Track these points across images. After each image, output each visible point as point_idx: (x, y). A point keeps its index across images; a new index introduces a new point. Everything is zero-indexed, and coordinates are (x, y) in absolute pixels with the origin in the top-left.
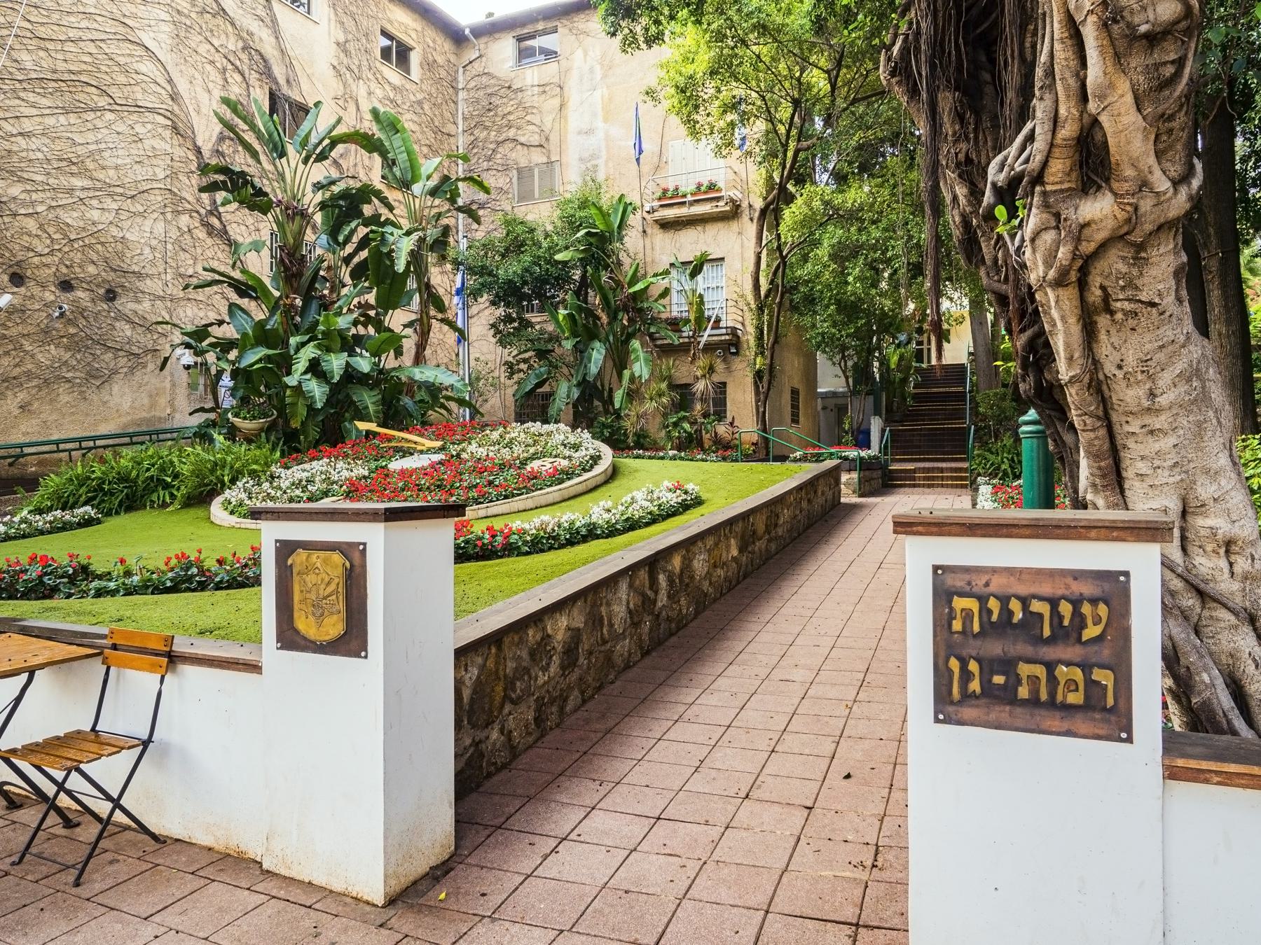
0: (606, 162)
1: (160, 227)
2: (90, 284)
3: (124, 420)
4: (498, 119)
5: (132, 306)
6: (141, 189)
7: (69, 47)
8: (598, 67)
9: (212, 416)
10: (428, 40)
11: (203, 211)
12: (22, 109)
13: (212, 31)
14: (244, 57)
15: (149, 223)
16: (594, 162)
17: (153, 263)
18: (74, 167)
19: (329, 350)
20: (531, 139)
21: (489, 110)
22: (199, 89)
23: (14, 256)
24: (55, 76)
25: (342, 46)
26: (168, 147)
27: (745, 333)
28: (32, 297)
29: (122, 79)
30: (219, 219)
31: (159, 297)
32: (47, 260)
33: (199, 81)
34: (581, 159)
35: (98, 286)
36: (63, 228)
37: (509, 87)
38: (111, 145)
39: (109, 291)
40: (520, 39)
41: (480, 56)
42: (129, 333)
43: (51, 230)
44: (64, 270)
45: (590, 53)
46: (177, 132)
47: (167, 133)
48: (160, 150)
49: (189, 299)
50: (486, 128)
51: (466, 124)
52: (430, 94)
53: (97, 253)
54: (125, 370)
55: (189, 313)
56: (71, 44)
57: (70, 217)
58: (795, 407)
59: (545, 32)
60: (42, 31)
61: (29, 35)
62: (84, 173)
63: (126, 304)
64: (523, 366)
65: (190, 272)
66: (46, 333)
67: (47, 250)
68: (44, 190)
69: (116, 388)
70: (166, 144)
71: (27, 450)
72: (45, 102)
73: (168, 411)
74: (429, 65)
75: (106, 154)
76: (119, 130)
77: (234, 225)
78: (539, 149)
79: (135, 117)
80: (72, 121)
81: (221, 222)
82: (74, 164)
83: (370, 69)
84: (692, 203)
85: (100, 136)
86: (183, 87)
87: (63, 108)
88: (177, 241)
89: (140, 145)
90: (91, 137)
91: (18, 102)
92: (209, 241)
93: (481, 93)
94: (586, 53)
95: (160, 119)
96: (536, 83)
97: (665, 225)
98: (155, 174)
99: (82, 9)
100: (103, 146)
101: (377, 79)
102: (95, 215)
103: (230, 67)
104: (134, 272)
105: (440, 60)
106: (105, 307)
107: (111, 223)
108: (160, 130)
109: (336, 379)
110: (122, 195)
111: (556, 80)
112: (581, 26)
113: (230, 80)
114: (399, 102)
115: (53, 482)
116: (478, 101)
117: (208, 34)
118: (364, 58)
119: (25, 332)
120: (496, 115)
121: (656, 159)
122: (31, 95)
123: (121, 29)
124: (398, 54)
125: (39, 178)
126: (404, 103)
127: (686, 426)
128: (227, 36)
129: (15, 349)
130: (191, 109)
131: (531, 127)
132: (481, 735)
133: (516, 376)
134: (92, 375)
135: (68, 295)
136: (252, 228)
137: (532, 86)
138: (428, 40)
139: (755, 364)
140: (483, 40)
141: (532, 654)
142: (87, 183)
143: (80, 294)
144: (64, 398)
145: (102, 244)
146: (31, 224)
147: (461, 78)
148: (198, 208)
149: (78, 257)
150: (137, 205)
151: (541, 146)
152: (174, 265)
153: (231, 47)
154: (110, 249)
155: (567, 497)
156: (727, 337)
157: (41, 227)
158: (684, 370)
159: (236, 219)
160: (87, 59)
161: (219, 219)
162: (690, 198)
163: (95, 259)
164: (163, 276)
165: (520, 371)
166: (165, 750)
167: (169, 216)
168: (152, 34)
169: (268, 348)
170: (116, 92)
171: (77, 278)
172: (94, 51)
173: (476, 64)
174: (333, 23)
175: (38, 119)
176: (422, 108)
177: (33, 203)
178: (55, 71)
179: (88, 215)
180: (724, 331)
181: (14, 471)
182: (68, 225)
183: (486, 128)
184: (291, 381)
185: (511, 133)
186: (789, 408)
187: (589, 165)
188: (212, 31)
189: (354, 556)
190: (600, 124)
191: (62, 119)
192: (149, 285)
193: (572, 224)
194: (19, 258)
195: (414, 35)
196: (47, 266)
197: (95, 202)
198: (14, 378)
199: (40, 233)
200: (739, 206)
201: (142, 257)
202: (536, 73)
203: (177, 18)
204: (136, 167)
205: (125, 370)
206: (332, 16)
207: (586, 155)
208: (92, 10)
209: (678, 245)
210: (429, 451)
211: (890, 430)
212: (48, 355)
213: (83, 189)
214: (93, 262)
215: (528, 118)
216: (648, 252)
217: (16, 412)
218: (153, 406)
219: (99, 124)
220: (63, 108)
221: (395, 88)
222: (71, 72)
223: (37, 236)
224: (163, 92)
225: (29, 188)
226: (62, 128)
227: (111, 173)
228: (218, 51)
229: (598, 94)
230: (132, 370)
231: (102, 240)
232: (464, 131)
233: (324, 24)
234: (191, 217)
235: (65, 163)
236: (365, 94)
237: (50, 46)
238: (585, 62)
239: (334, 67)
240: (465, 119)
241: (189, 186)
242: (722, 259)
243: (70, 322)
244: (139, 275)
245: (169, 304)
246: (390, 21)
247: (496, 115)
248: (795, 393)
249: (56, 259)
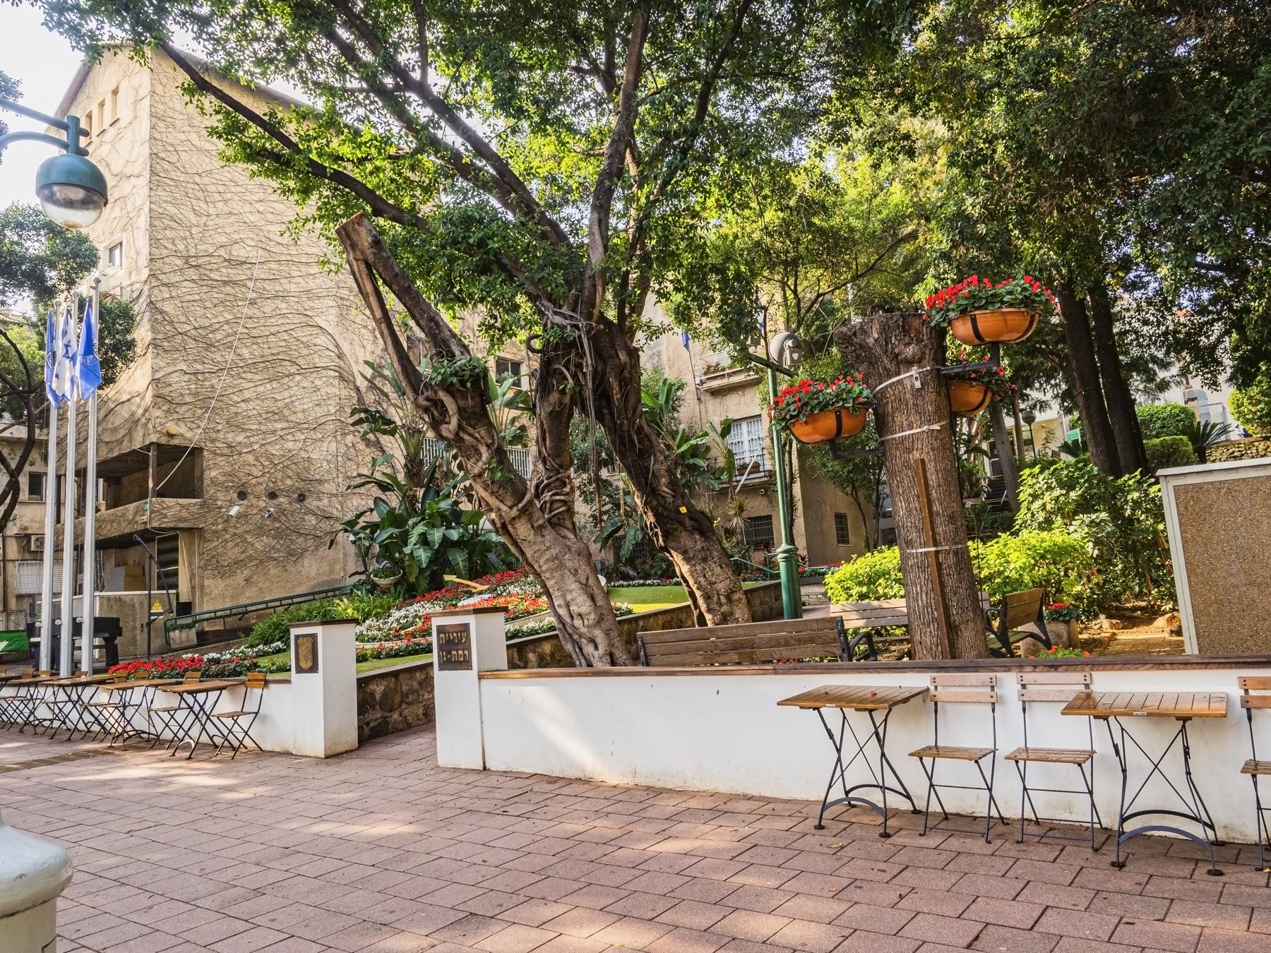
1: (333, 446)
2: (289, 490)
3: (313, 583)
5: (315, 503)
7: (272, 338)
9: (363, 577)
15: (325, 444)
17: (329, 472)
19: (433, 526)
22: (357, 347)
29: (305, 352)
36: (269, 457)
39: (300, 495)
43: (263, 460)
46: (341, 377)
55: (355, 503)
57: (274, 450)
60: (255, 333)
63: (312, 503)
69: (306, 562)
70: (337, 390)
71: (250, 609)
72: (258, 377)
79: (314, 375)
84: (730, 375)
86: (345, 348)
90: (286, 394)
92: (368, 451)
95: (332, 373)
97: (715, 393)
102: (290, 445)
109: (437, 546)
115: (260, 628)
123: (304, 319)
125: (254, 427)
132: (386, 714)
134: (291, 553)
141: (420, 684)
142: (285, 425)
143: (281, 499)
144: (273, 572)
149: (279, 475)
157: (257, 459)
160: (283, 344)
162: (728, 371)
166: (265, 718)
170: (301, 361)
172: (286, 337)
177: (251, 444)
181: (242, 623)
184: (407, 550)
186: (834, 531)
189: (314, 637)
191: (268, 386)
192: (329, 487)
196: (260, 484)
197: (290, 437)
203: (340, 302)
210: (481, 593)
212: (262, 543)
218: (331, 571)
219: (291, 384)
227: (300, 415)
230: (317, 548)
237: (259, 340)
243: (276, 520)
244: (320, 482)
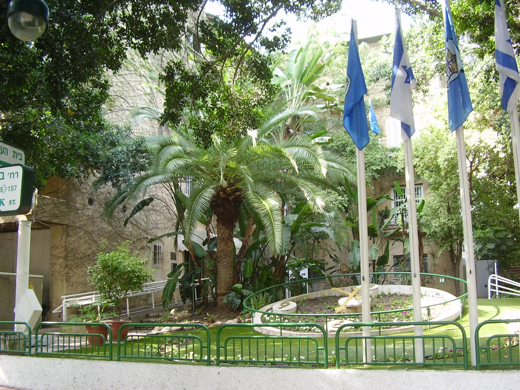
26: (148, 127)
42: (131, 229)
80: (114, 116)
249: (105, 189)
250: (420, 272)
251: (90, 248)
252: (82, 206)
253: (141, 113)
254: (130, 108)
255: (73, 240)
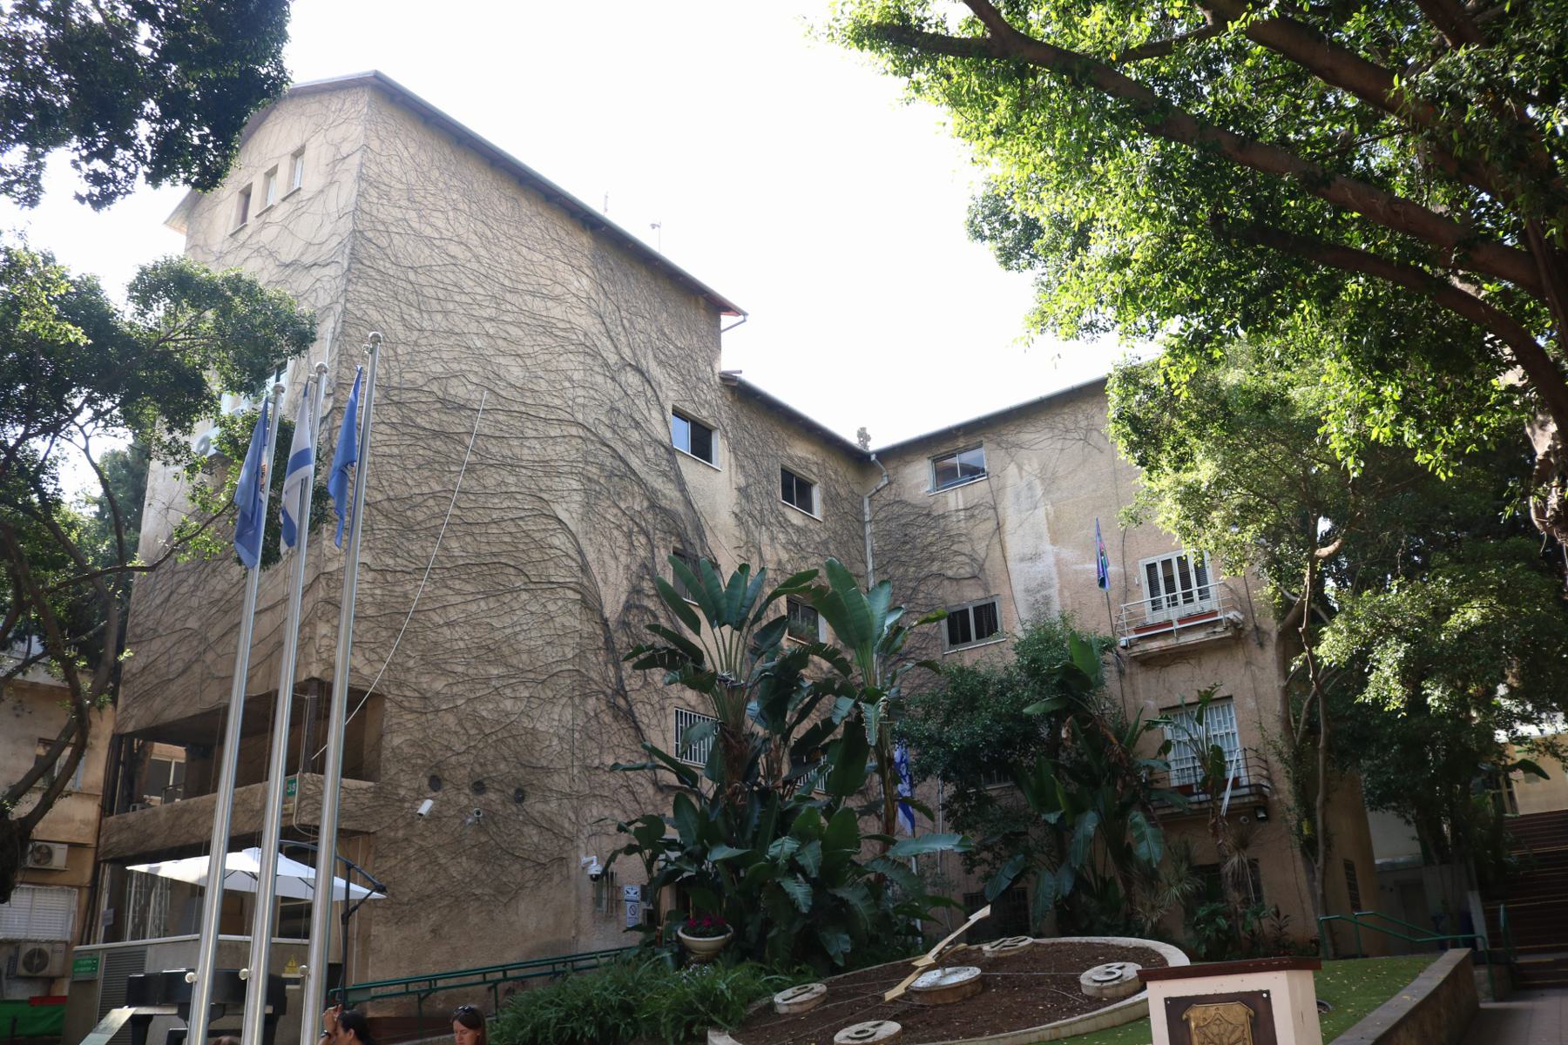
0: (1061, 592)
4: (916, 552)
5: (539, 806)
6: (552, 672)
8: (1038, 482)
10: (830, 472)
11: (609, 691)
12: (449, 598)
13: (619, 494)
14: (649, 517)
15: (557, 709)
16: (1044, 593)
18: (491, 655)
20: (962, 571)
21: (905, 543)
23: (434, 756)
24: (478, 560)
25: (743, 491)
26: (577, 623)
27: (1275, 791)
28: (448, 801)
29: (536, 555)
30: (625, 698)
31: (566, 794)
32: (463, 759)
33: (607, 549)
34: (1027, 591)
35: (509, 786)
36: (479, 722)
37: (928, 515)
38: (525, 627)
40: (935, 460)
41: (890, 483)
42: (536, 839)
43: (468, 725)
44: (478, 769)
45: (1026, 467)
47: (576, 609)
48: (569, 627)
49: (595, 796)
50: (903, 564)
51: (877, 561)
52: (835, 532)
53: (509, 747)
54: (532, 884)
56: (493, 525)
57: (485, 710)
58: (1352, 886)
59: (966, 450)
60: (471, 517)
61: (458, 521)
62: (501, 660)
63: (534, 806)
64: (985, 855)
65: (597, 762)
66: (459, 842)
67: (464, 748)
68: (463, 682)
69: (522, 906)
70: (575, 621)
72: (469, 588)
73: (573, 933)
74: (831, 500)
75: (520, 637)
76: (533, 609)
77: (639, 705)
78: (972, 582)
79: (547, 594)
80: (492, 606)
81: (627, 702)
82: (492, 651)
83: (772, 512)
85: (515, 619)
87: (484, 593)
88: (584, 729)
89: (551, 625)
90: (507, 620)
91: (445, 590)
92: (615, 726)
93: (893, 524)
94: (1020, 468)
96: (961, 507)
98: (564, 655)
99: (504, 489)
100: (518, 629)
101: (779, 522)
102: (508, 705)
103: (636, 529)
104: (542, 768)
105: (842, 492)
106: (514, 809)
107: (522, 712)
108: (570, 606)
110: (533, 680)
111: (989, 499)
112: (1012, 438)
113: (636, 543)
114: (803, 545)
116: (889, 533)
117: (616, 497)
118: (766, 501)
119: (441, 842)
120: (914, 548)
121: (1123, 583)
122: (457, 582)
123: (537, 504)
124: (796, 489)
125: (460, 669)
126: (808, 546)
127: (1222, 922)
128: (634, 497)
129: (430, 863)
130: (599, 579)
131: (959, 558)
133: (977, 869)
135: (481, 798)
136: (657, 706)
137: (957, 511)
138: (830, 472)
139: (1302, 831)
140: (893, 464)
142: (501, 670)
144: (474, 919)
145: (514, 737)
146: (451, 720)
147: (867, 510)
148: (605, 688)
150: (547, 691)
151: (974, 577)
152: (580, 756)
153: (637, 508)
154: (521, 743)
155: (1131, 990)
156: (1252, 799)
157: (460, 723)
158: (1203, 848)
159: (641, 698)
161: (625, 698)
162: (1177, 626)
163: (506, 755)
164: (570, 770)
165: (984, 861)
167: (577, 701)
168: (565, 506)
169: (730, 845)
171: (490, 778)
172: (514, 530)
173: (885, 493)
174: (734, 468)
175: (462, 607)
176: (828, 549)
177: (454, 697)
178: (478, 555)
179: (502, 706)
180: (1246, 791)
182: (483, 718)
183: (903, 564)
185: (935, 567)
187: (1038, 596)
188: (619, 494)
190: (1047, 547)
193: (1033, 669)
194: (439, 758)
195: (815, 470)
196: (463, 765)
197: (508, 691)
198: (428, 896)
199: (458, 729)
200: (1242, 629)
201: (551, 750)
202: (960, 495)
204: (548, 648)
205: (532, 884)
206: (733, 460)
207: (1034, 585)
208: (513, 489)
209: (1167, 685)
211: (1506, 909)
213: (499, 677)
214: (505, 759)
215: (955, 547)
216: (1128, 696)
217: (428, 937)
220: (484, 593)
221: (798, 530)
222: (493, 554)
223: (456, 733)
224: (574, 564)
225: (451, 681)
226: (482, 614)
227: (524, 657)
228: (624, 513)
229: (1041, 513)
231: (514, 732)
232: (874, 569)
233: (725, 470)
234: (598, 699)
235: (483, 651)
236: (768, 542)
238: (1022, 478)
239: (736, 515)
240: (874, 555)
241: (598, 668)
242: (1230, 697)
244: (547, 771)
245: (575, 802)
246: (790, 458)
247: (914, 548)
248: (1349, 866)
249: (471, 757)
250: (976, 609)
251: (432, 881)
252: (414, 794)
253: (578, 918)
254: (532, 586)
255: (388, 864)
